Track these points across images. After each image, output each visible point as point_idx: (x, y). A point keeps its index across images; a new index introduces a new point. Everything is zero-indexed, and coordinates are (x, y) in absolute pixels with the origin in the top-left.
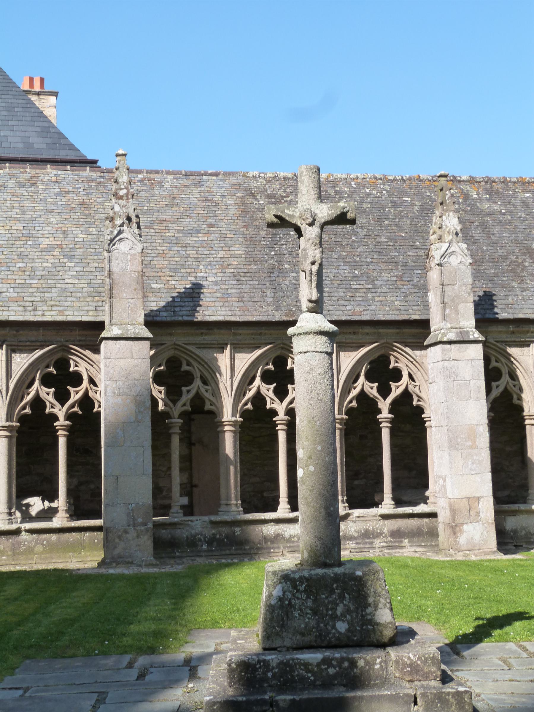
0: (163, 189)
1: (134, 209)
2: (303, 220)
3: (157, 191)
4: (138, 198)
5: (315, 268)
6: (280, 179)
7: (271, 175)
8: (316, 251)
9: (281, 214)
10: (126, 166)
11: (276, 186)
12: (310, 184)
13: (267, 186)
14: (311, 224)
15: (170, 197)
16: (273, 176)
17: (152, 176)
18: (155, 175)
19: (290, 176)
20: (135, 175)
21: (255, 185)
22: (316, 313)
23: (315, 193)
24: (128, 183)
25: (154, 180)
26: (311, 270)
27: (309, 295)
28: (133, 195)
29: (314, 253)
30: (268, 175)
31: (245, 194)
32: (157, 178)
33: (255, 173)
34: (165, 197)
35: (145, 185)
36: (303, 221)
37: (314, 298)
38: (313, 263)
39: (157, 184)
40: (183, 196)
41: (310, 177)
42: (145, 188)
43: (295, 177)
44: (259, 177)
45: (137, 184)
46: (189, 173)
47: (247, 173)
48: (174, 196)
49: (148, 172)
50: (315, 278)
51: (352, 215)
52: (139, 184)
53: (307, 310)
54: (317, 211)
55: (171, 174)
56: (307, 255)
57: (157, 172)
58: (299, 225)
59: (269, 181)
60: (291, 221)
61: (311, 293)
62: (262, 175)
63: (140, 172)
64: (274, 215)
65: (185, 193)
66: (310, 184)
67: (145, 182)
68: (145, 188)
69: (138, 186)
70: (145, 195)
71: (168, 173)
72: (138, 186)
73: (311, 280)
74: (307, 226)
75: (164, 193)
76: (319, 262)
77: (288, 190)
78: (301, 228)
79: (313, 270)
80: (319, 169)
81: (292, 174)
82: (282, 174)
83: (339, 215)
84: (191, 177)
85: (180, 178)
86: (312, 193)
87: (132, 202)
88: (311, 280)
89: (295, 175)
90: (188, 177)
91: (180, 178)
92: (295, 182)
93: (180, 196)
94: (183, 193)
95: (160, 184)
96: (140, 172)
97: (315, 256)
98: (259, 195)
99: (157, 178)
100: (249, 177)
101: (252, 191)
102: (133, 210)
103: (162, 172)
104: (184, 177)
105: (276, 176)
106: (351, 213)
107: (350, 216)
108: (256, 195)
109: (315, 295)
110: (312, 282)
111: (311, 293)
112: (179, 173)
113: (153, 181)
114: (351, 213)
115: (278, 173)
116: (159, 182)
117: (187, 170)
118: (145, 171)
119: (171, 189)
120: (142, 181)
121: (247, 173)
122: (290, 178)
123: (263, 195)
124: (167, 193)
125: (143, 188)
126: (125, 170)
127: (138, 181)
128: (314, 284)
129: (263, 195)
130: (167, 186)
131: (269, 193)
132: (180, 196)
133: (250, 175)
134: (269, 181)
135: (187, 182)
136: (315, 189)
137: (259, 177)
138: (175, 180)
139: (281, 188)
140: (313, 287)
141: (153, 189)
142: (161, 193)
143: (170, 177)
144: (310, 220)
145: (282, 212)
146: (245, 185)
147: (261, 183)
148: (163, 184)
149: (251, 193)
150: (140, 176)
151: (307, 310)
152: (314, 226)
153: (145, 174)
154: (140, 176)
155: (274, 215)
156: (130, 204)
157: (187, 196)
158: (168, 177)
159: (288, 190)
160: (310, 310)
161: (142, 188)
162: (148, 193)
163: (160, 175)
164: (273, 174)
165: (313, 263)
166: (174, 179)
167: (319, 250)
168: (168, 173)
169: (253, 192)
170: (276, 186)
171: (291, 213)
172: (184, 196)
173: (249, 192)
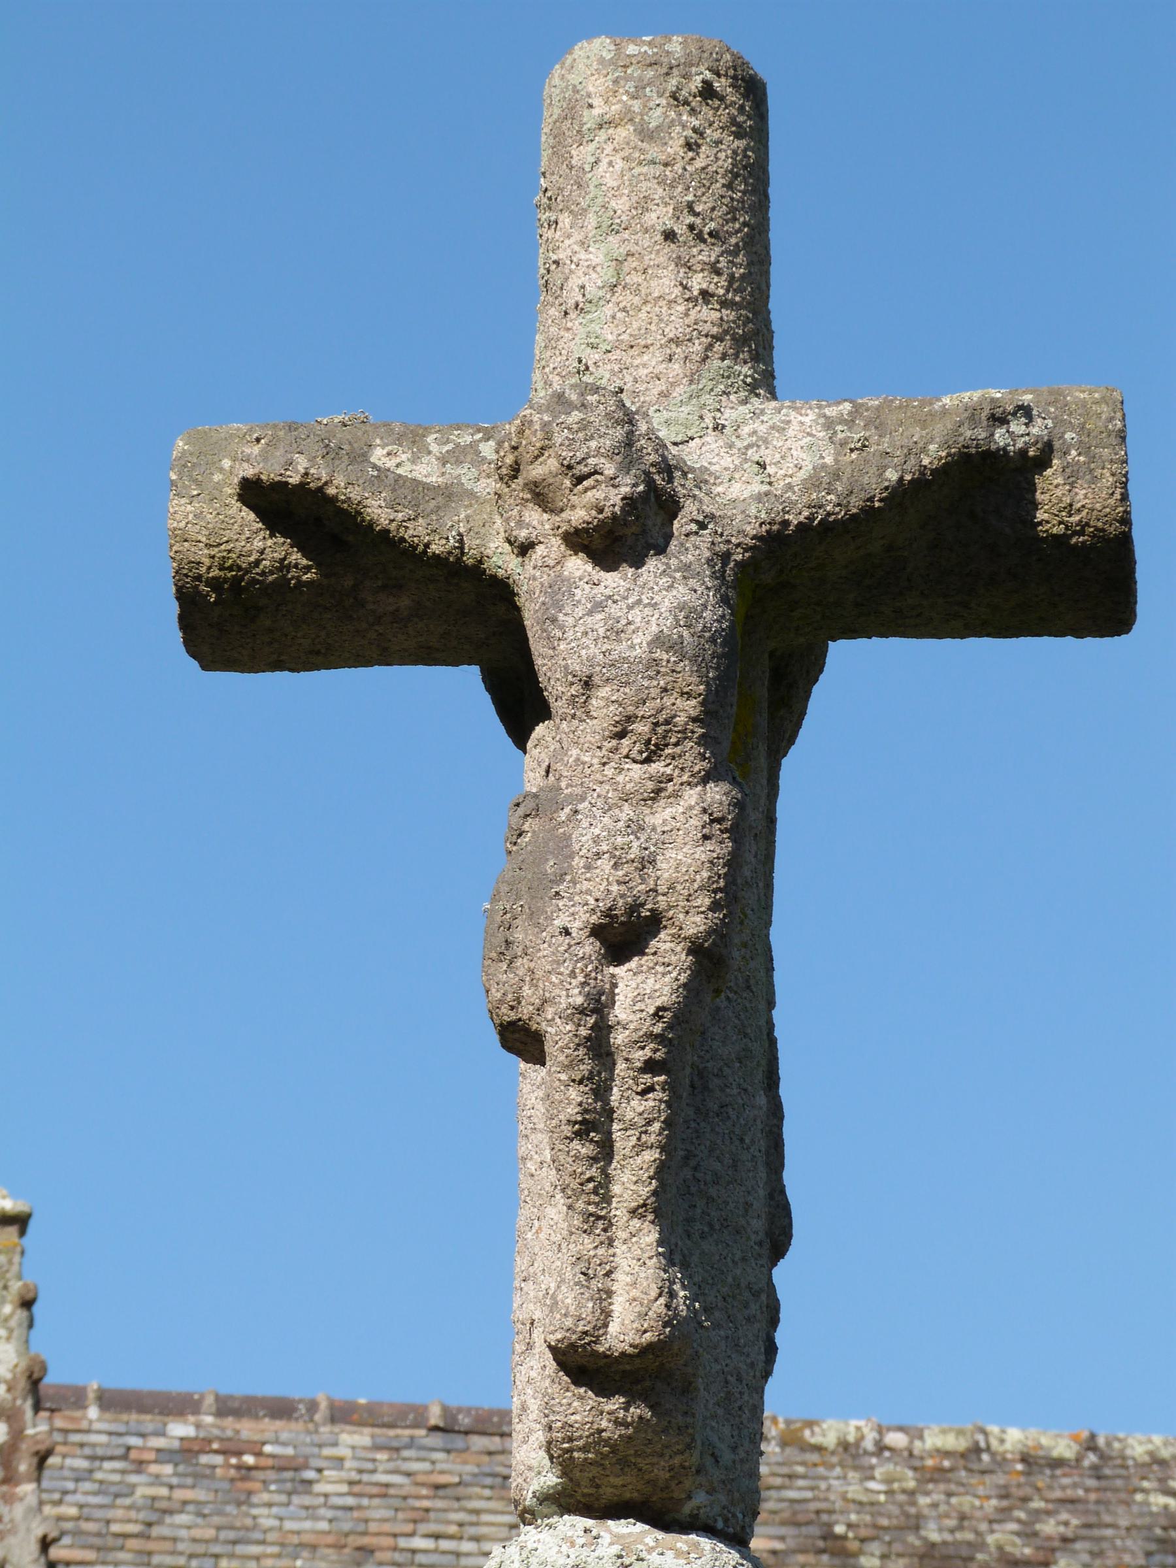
0: (307, 1500)
1: (45, 1544)
2: (540, 496)
3: (268, 1511)
4: (151, 1546)
5: (644, 989)
6: (1000, 1462)
7: (951, 1442)
8: (662, 815)
9: (321, 472)
10: (16, 1286)
11: (979, 1499)
12: (643, 205)
13: (923, 1501)
14: (619, 541)
15: (340, 1547)
16: (962, 1444)
17: (247, 1429)
18: (269, 1426)
19: (1064, 1449)
20: (149, 1422)
21: (854, 1491)
22: (664, 1516)
23: (698, 282)
24: (23, 1384)
25: (259, 1454)
26: (598, 1005)
27: (568, 1298)
28: (42, 1458)
29: (635, 827)
30: (933, 1440)
31: (791, 1543)
32: (279, 1439)
33: (856, 1426)
34: (314, 1547)
35: (201, 1476)
36: (534, 516)
37: (627, 1327)
38: (624, 935)
39: (271, 1475)
40: (419, 1543)
41: (646, 134)
42: (200, 1494)
43: (1092, 1458)
44: (881, 1448)
45: (154, 1468)
46: (464, 1421)
47: (810, 1424)
48: (365, 1541)
49: (226, 1408)
50: (636, 1108)
51: (1082, 495)
52: (168, 1469)
53: (551, 1479)
54: (704, 454)
55: (362, 1424)
56: (563, 847)
57: (282, 1409)
58: (501, 559)
59: (938, 1475)
60: (417, 532)
61: (596, 1278)
62: (896, 1439)
63: (183, 1406)
64: (253, 493)
65: (433, 1528)
66: (643, 205)
67: (204, 1459)
68: (200, 1494)
69: (157, 1480)
70: (197, 1533)
71: (342, 1414)
72: (157, 1480)
73: (594, 1126)
74: (578, 565)
75: (307, 1525)
76: (695, 924)
77: (1049, 1527)
78: (522, 590)
79: (621, 1012)
80: (753, 89)
81: (1075, 1438)
82: (1014, 1438)
83: (943, 472)
84: (479, 1442)
85: (411, 1443)
86: (665, 282)
87: (32, 1500)
88: (594, 1126)
89: (1091, 1445)
90: (459, 1442)
91: (411, 1443)
92: (1091, 1483)
93: (403, 1543)
94: (423, 1528)
95: (294, 1474)
96: (183, 1406)
97: (646, 862)
98: (875, 1548)
99: (276, 1442)
100: (819, 1448)
101: (830, 1525)
102: (34, 1547)
103: (313, 1406)
104: (437, 1440)
105: (976, 1450)
106: (1072, 476)
107: (1063, 499)
108: (853, 1546)
109: (635, 1299)
110: (606, 1151)
111: (596, 1278)
112: (413, 1415)
113: (249, 1459)
114: (1072, 476)
115: (994, 1429)
116: (282, 1466)
117: (453, 1403)
118: (210, 1400)
119: (350, 1501)
120: (187, 1452)
121: (810, 1424)
122: (1058, 1463)
123: (897, 1547)
124: (323, 1526)
125: (189, 1494)
126: (8, 1309)
127: (163, 1455)
128: (632, 1177)
129: (897, 1547)
130: (331, 1484)
131: (935, 1537)
132: (403, 1543)
133: (828, 1434)
134: (938, 1475)
135: (449, 1468)
136: (707, 254)
137: (881, 1448)
138: (382, 1456)
139: (1003, 1515)
140: (619, 1212)
141: (245, 1500)
142: (289, 1525)
143: (353, 1439)
144: (610, 495)
145: (330, 453)
146: (792, 1494)
147: (888, 1481)
148: (310, 1475)
149: (829, 1536)
150: (180, 1429)
151: (551, 1479)
152: (653, 564)
153: (209, 1419)
154: (180, 1429)
155: (253, 493)
156: (18, 1510)
157: (445, 1545)
158: (346, 1438)
159: (1049, 1527)
160: (589, 1490)
161: (179, 1494)
162: (216, 1520)
163: (298, 1426)
164: (960, 1433)
165: (624, 935)
166: (377, 1448)
167: (691, 796)
168: (342, 1414)
169: (839, 1529)
170: (979, 1499)
171: (427, 471)
172: (428, 1544)
173: (814, 1530)
